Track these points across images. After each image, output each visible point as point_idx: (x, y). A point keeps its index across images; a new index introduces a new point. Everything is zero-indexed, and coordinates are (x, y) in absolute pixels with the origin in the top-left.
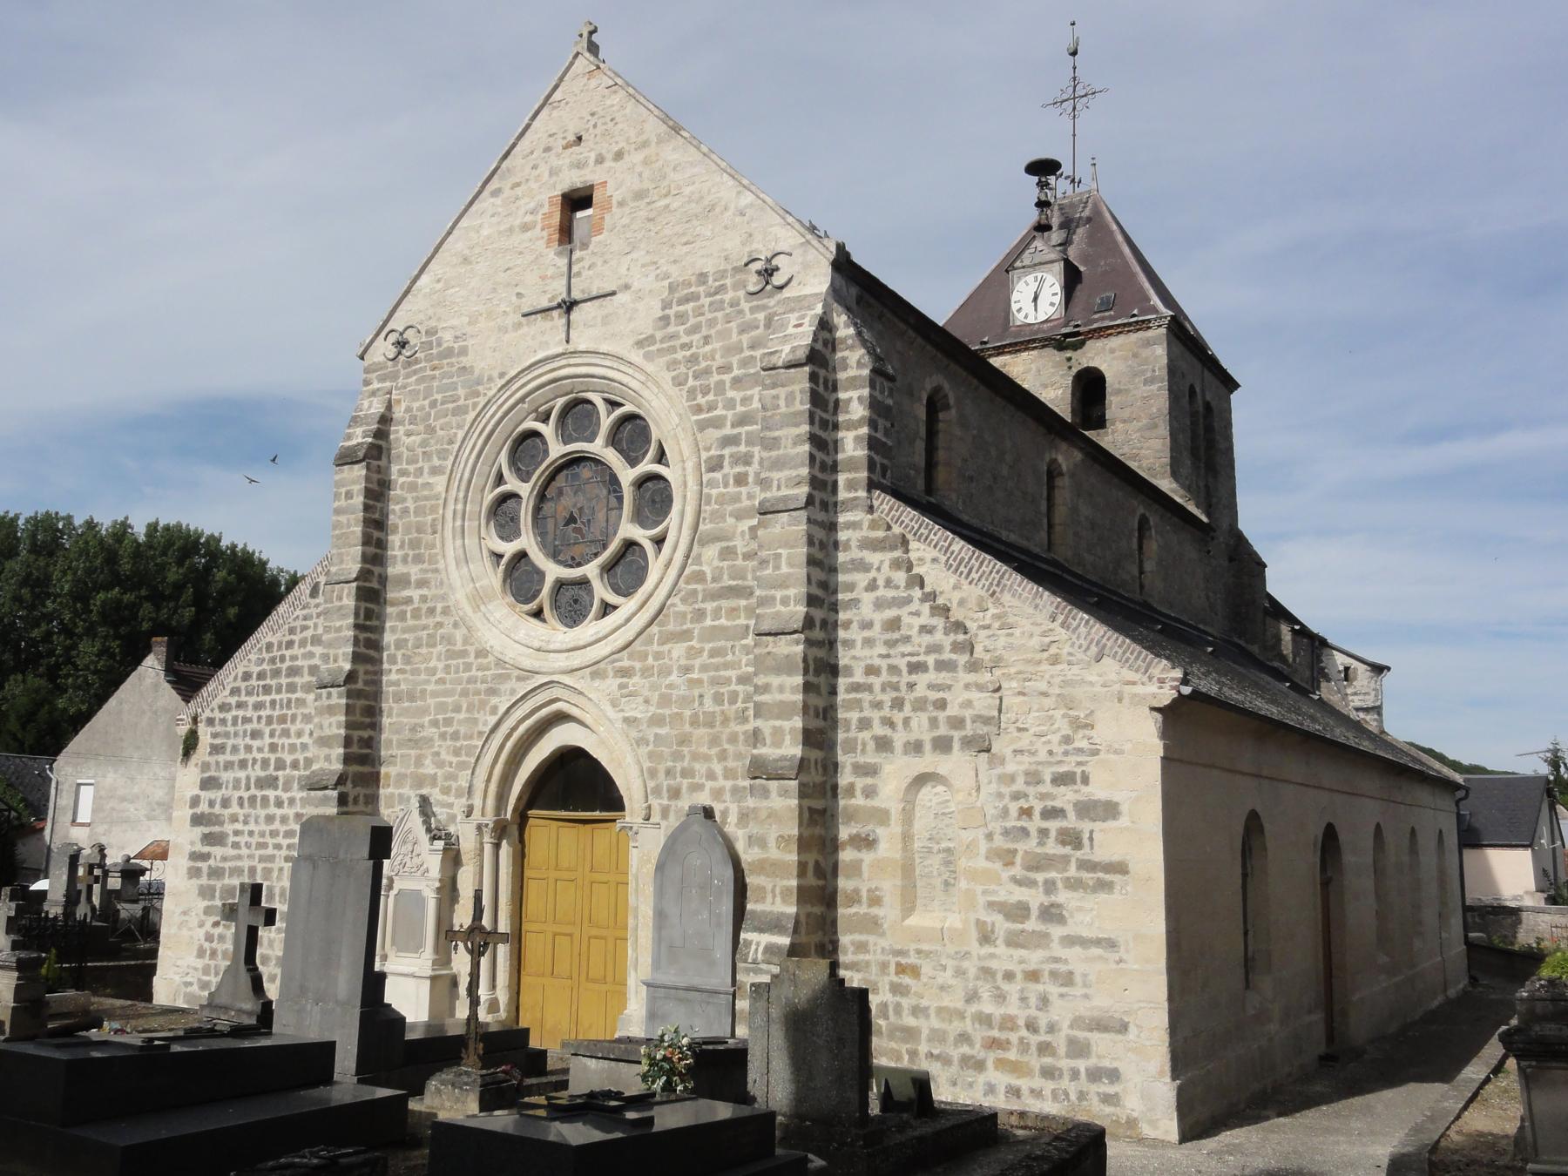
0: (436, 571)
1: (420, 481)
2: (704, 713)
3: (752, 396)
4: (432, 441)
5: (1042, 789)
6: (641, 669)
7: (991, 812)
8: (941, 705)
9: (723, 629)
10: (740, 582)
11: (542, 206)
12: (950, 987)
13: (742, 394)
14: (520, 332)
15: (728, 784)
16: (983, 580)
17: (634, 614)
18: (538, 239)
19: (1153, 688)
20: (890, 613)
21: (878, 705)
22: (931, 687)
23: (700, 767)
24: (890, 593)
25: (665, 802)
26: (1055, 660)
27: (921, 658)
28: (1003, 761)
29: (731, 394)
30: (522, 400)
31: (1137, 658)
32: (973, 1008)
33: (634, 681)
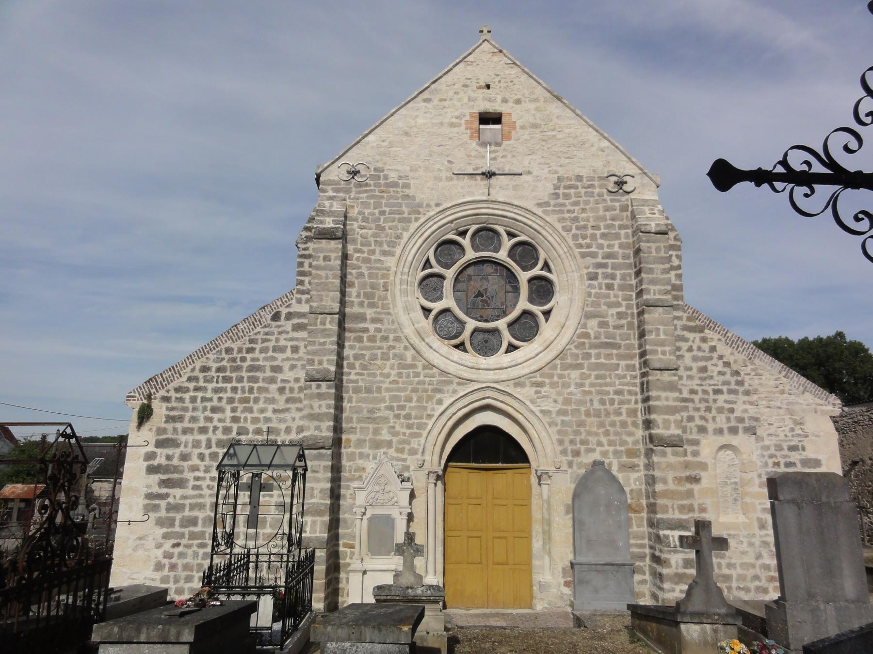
0: (389, 314)
1: (373, 258)
2: (594, 410)
3: (614, 245)
4: (383, 235)
5: (783, 453)
6: (549, 383)
7: (759, 464)
8: (732, 411)
9: (602, 365)
10: (612, 340)
11: (464, 116)
12: (747, 552)
13: (608, 242)
14: (451, 183)
15: (611, 449)
16: (745, 352)
17: (541, 352)
18: (463, 134)
19: (830, 408)
20: (702, 364)
21: (697, 409)
22: (726, 402)
23: (593, 439)
24: (700, 354)
25: (570, 458)
26: (782, 392)
27: (720, 387)
28: (763, 440)
29: (600, 241)
30: (451, 222)
31: (821, 394)
32: (760, 562)
33: (545, 390)
